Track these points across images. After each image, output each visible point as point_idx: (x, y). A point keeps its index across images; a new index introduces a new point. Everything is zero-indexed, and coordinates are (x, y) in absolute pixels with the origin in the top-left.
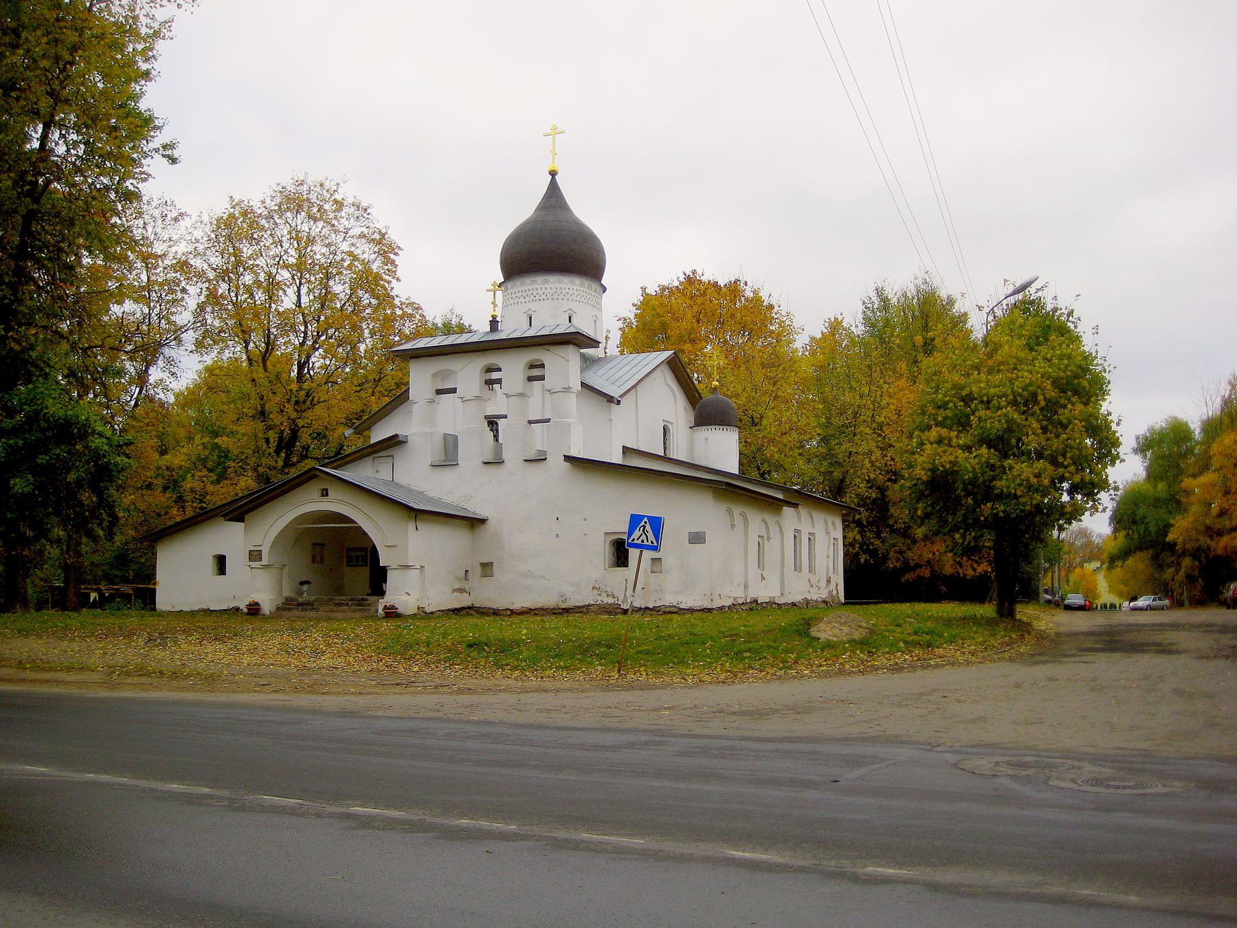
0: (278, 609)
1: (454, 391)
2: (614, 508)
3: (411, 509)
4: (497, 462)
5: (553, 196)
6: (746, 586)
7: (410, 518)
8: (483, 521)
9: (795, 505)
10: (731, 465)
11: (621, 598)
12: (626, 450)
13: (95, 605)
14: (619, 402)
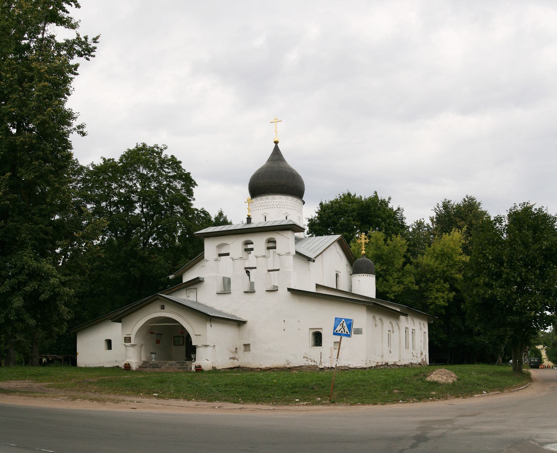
0: (140, 367)
1: (228, 254)
2: (324, 317)
3: (209, 315)
4: (251, 291)
5: (276, 152)
6: (382, 356)
7: (207, 320)
8: (244, 322)
9: (406, 315)
10: (372, 294)
11: (319, 362)
12: (318, 286)
13: (44, 365)
14: (314, 261)
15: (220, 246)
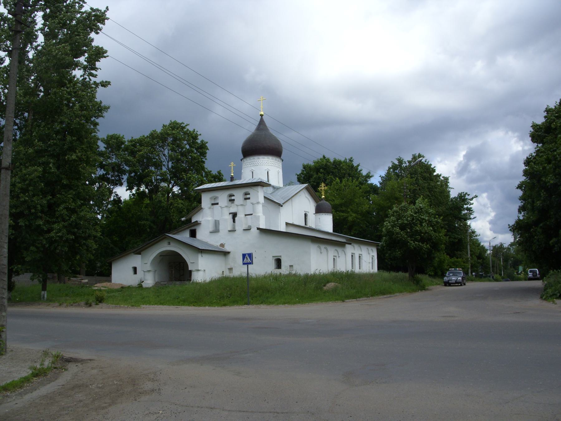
1: (217, 204)
8: (229, 253)
9: (350, 244)
12: (287, 224)
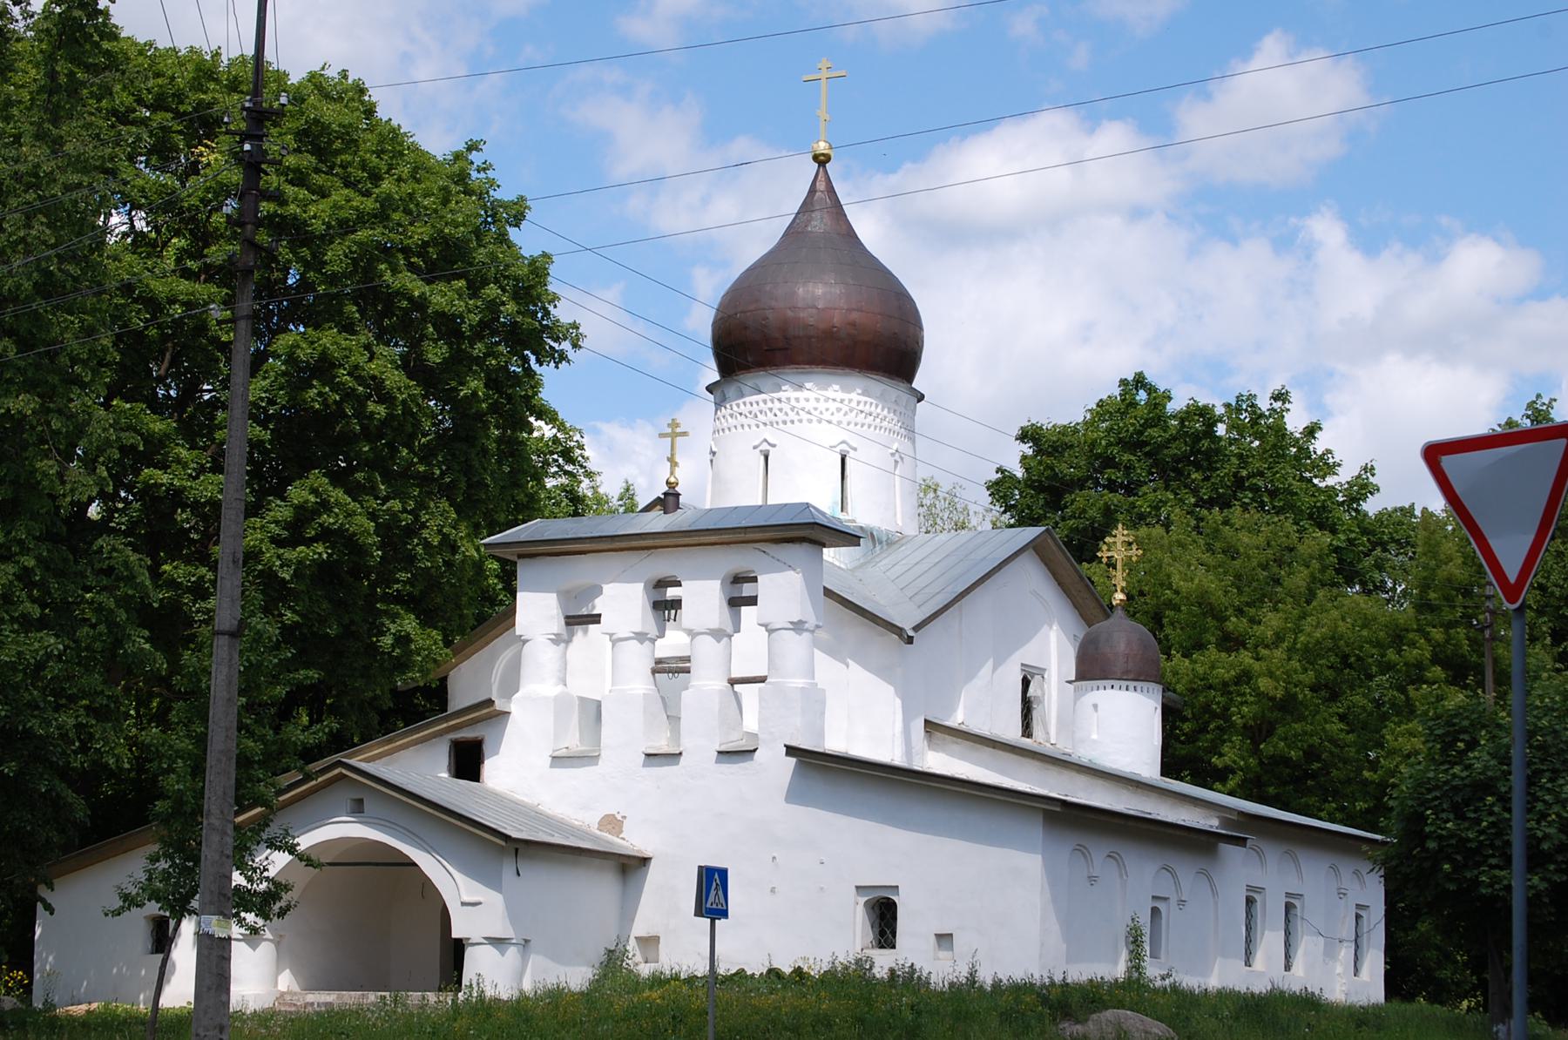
1: (596, 619)
3: (507, 838)
8: (645, 861)
9: (1241, 842)
14: (910, 640)
15: (566, 597)
